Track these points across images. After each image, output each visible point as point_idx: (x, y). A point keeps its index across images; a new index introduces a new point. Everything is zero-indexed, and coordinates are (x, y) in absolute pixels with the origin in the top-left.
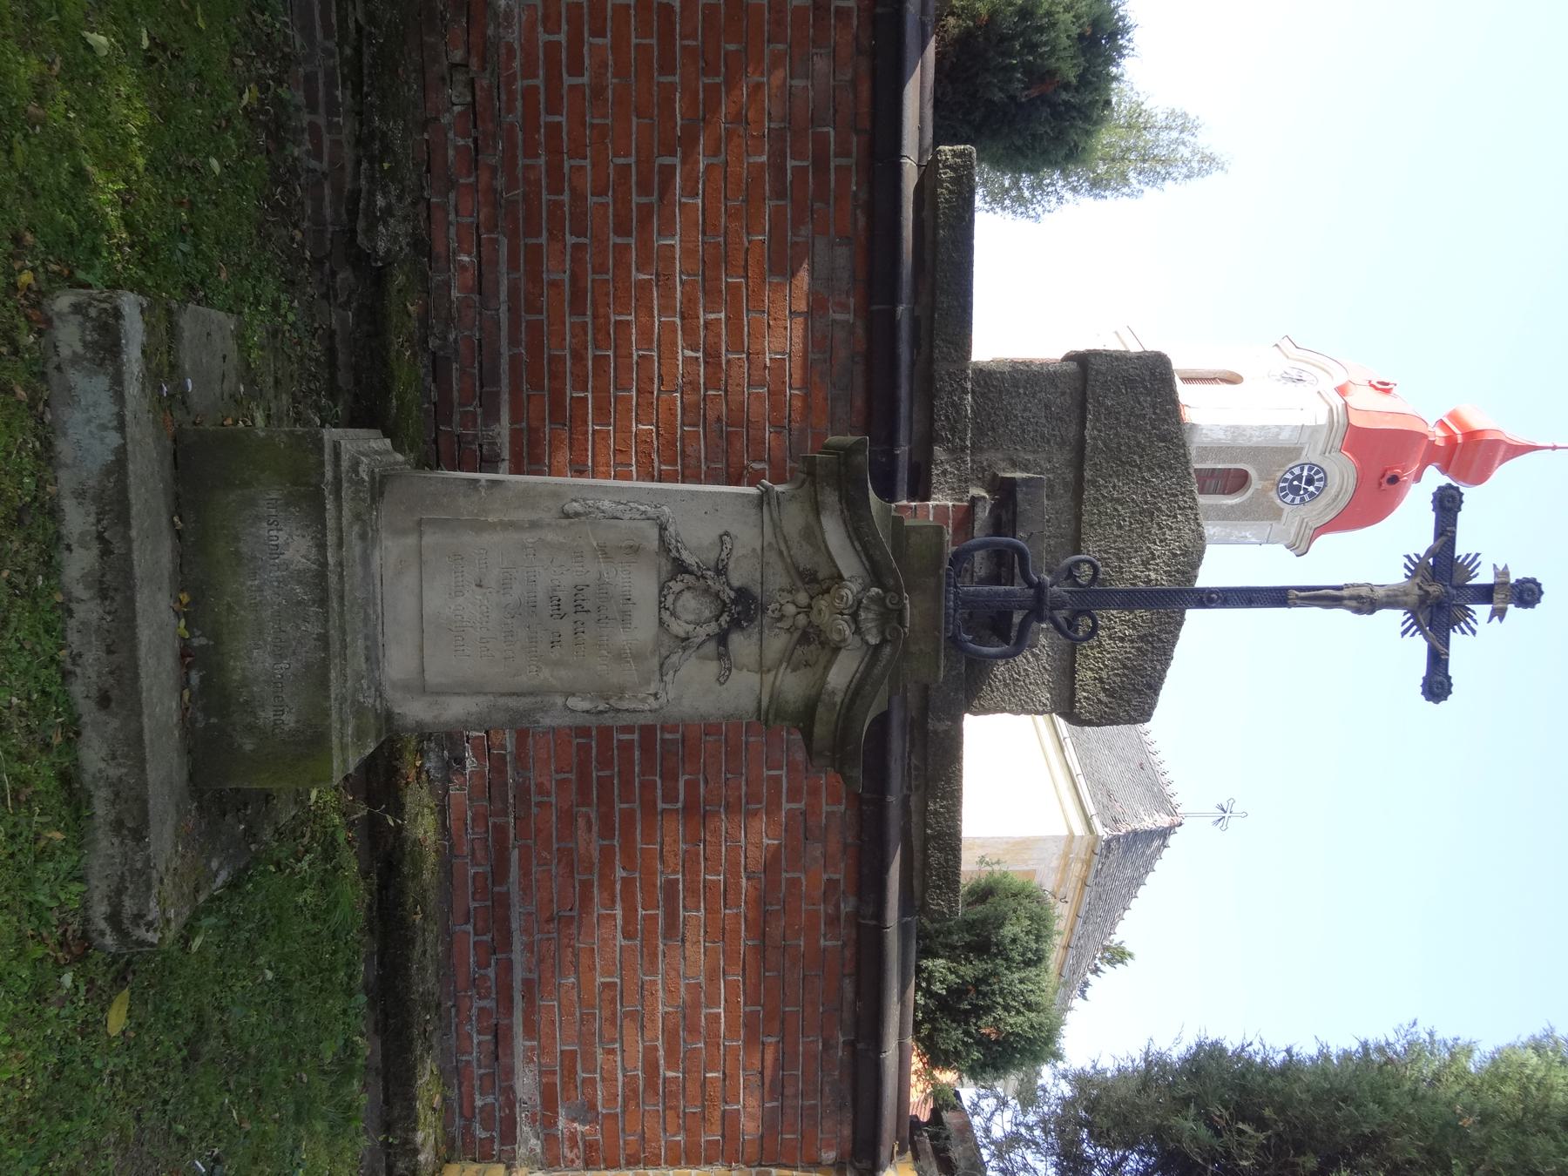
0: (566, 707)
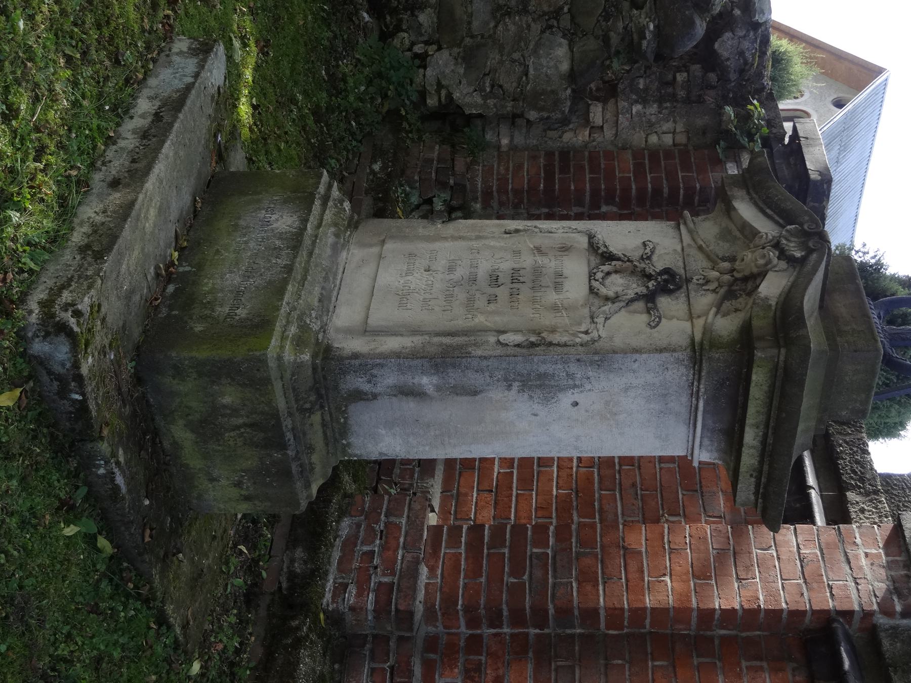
0: (499, 342)
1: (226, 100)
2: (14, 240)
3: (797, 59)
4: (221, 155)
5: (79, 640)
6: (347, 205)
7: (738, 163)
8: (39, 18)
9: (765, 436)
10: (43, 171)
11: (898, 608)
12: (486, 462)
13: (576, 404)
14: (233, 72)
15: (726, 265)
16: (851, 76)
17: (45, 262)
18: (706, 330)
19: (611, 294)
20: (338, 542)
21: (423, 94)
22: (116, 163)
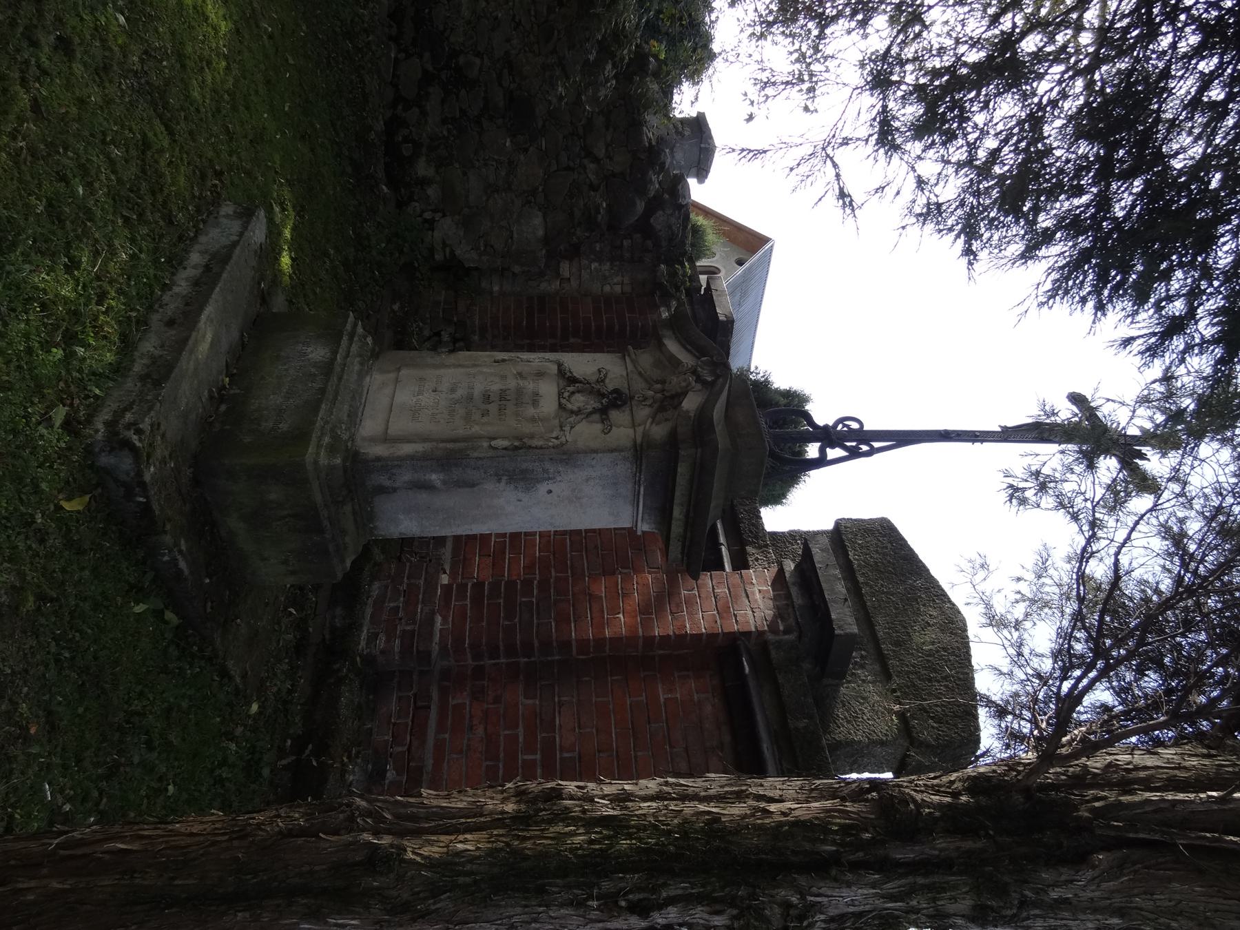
1: (269, 254)
2: (80, 371)
3: (709, 231)
4: (264, 298)
5: (151, 696)
6: (369, 340)
7: (668, 307)
8: (97, 185)
9: (688, 511)
10: (105, 313)
11: (781, 628)
12: (484, 538)
13: (550, 492)
14: (274, 231)
15: (659, 386)
16: (749, 244)
17: (109, 388)
18: (645, 435)
19: (575, 408)
20: (370, 601)
21: (432, 250)
22: (172, 304)
